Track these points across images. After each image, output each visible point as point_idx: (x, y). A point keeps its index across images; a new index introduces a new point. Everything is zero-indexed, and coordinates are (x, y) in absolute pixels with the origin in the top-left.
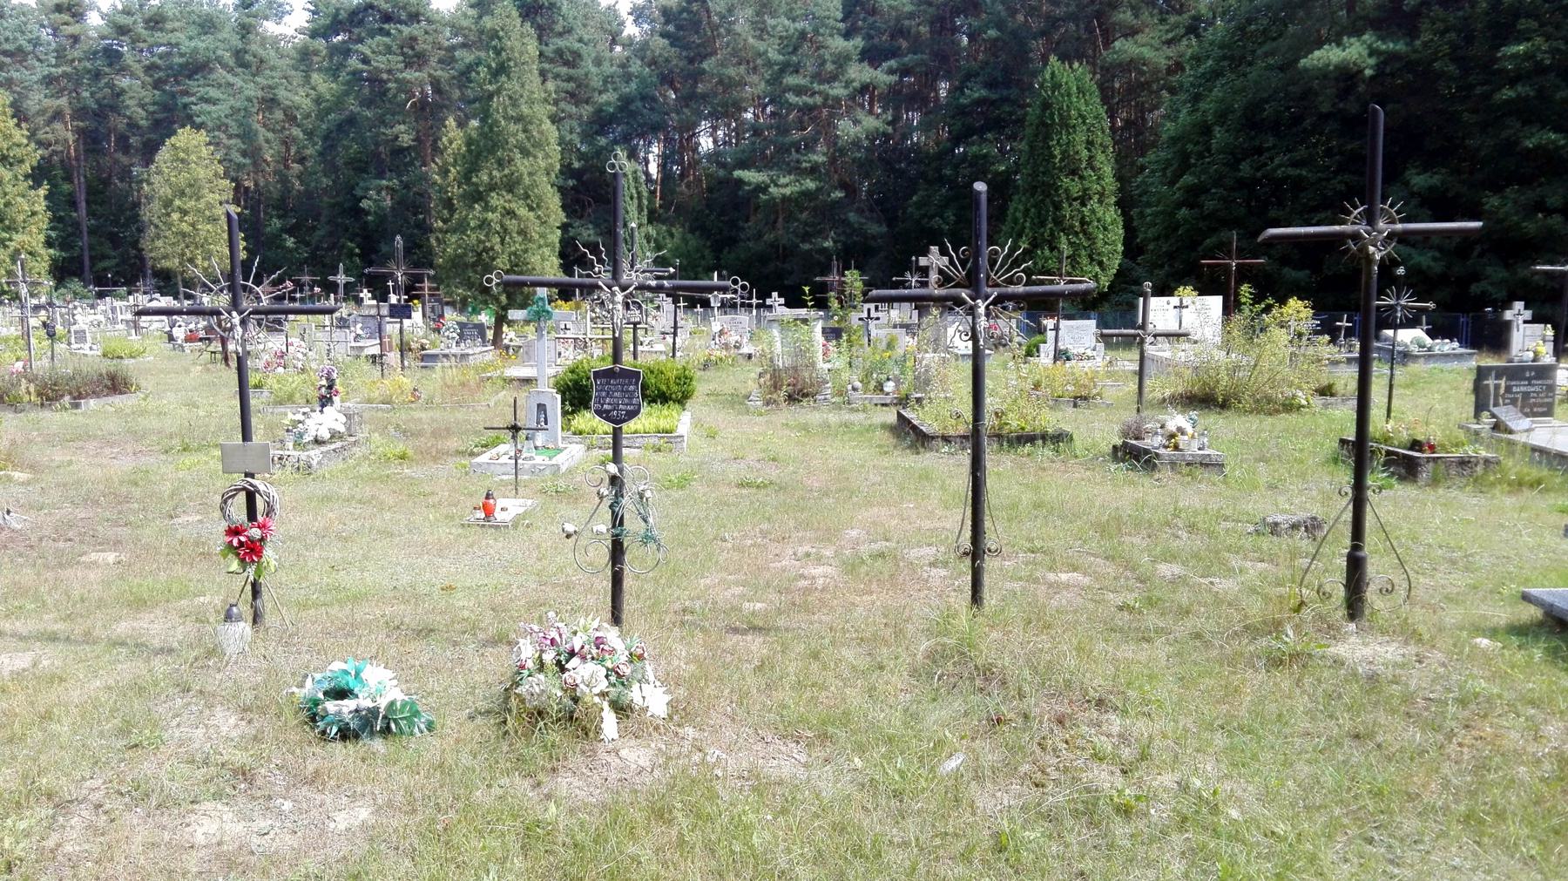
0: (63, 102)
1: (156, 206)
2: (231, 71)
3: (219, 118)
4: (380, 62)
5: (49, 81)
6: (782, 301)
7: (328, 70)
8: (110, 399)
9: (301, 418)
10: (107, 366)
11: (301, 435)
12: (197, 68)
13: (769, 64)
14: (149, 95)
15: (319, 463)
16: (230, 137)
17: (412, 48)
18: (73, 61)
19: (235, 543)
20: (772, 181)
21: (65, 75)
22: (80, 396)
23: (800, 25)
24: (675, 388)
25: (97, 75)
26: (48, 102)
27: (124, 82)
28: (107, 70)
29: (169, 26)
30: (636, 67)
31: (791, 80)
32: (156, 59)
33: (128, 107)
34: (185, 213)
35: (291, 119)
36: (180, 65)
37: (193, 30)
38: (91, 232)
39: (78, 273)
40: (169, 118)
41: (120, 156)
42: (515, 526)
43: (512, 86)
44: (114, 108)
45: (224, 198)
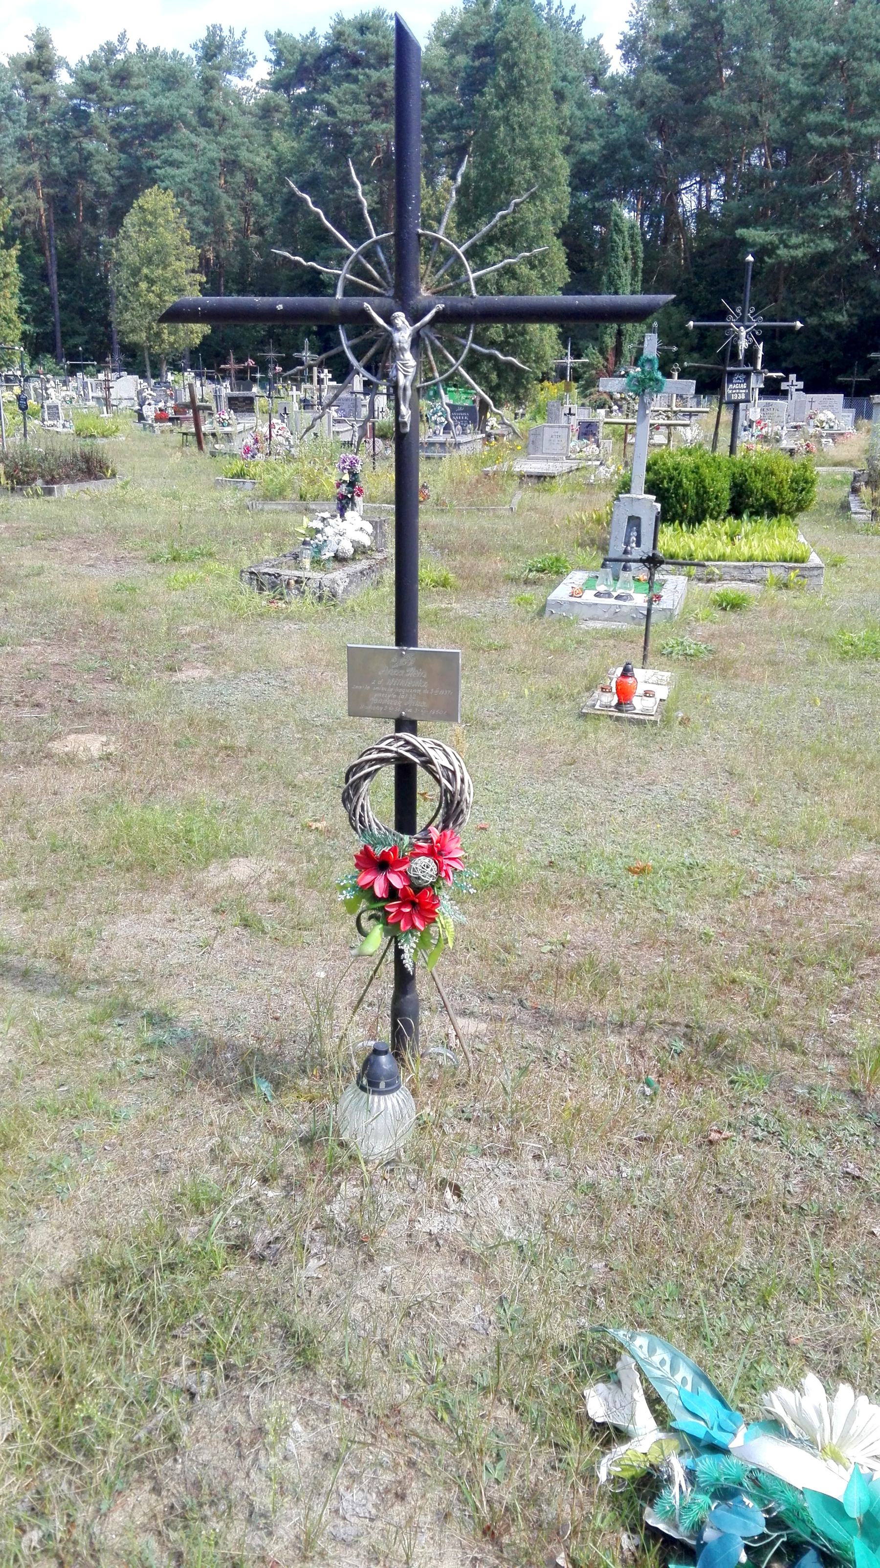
0: (35, 167)
1: (124, 274)
2: (194, 130)
3: (182, 183)
4: (346, 113)
5: (22, 144)
6: (801, 385)
7: (290, 125)
8: (85, 485)
9: (320, 525)
10: (81, 446)
11: (319, 549)
12: (161, 128)
13: (789, 96)
14: (116, 159)
15: (345, 590)
16: (193, 203)
17: (380, 96)
18: (43, 123)
19: (379, 889)
20: (782, 241)
21: (36, 139)
22: (53, 481)
23: (832, 48)
24: (790, 496)
25: (66, 138)
26: (20, 168)
27: (90, 145)
28: (75, 132)
29: (134, 82)
30: (623, 109)
31: (812, 118)
32: (121, 119)
33: (95, 173)
34: (152, 282)
35: (252, 183)
36: (145, 125)
37: (157, 86)
38: (64, 306)
39: (51, 349)
40: (135, 180)
41: (87, 226)
42: (667, 722)
43: (521, 111)
44: (82, 174)
45: (190, 266)
